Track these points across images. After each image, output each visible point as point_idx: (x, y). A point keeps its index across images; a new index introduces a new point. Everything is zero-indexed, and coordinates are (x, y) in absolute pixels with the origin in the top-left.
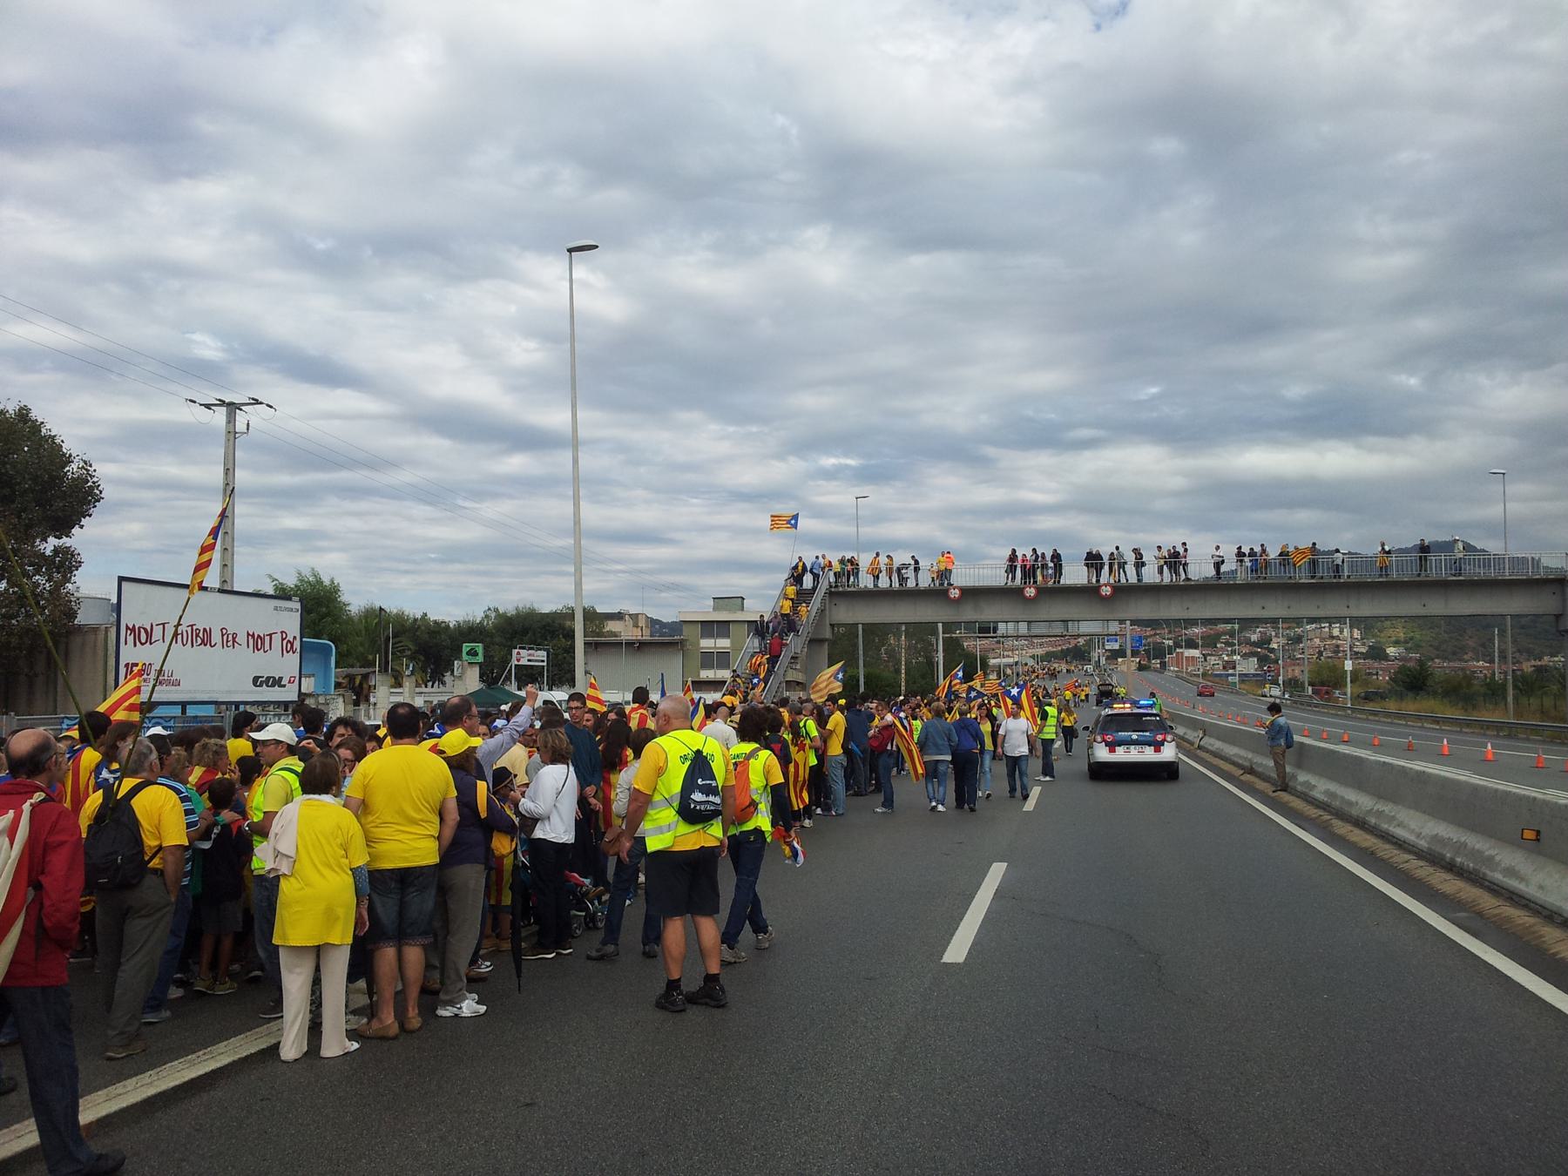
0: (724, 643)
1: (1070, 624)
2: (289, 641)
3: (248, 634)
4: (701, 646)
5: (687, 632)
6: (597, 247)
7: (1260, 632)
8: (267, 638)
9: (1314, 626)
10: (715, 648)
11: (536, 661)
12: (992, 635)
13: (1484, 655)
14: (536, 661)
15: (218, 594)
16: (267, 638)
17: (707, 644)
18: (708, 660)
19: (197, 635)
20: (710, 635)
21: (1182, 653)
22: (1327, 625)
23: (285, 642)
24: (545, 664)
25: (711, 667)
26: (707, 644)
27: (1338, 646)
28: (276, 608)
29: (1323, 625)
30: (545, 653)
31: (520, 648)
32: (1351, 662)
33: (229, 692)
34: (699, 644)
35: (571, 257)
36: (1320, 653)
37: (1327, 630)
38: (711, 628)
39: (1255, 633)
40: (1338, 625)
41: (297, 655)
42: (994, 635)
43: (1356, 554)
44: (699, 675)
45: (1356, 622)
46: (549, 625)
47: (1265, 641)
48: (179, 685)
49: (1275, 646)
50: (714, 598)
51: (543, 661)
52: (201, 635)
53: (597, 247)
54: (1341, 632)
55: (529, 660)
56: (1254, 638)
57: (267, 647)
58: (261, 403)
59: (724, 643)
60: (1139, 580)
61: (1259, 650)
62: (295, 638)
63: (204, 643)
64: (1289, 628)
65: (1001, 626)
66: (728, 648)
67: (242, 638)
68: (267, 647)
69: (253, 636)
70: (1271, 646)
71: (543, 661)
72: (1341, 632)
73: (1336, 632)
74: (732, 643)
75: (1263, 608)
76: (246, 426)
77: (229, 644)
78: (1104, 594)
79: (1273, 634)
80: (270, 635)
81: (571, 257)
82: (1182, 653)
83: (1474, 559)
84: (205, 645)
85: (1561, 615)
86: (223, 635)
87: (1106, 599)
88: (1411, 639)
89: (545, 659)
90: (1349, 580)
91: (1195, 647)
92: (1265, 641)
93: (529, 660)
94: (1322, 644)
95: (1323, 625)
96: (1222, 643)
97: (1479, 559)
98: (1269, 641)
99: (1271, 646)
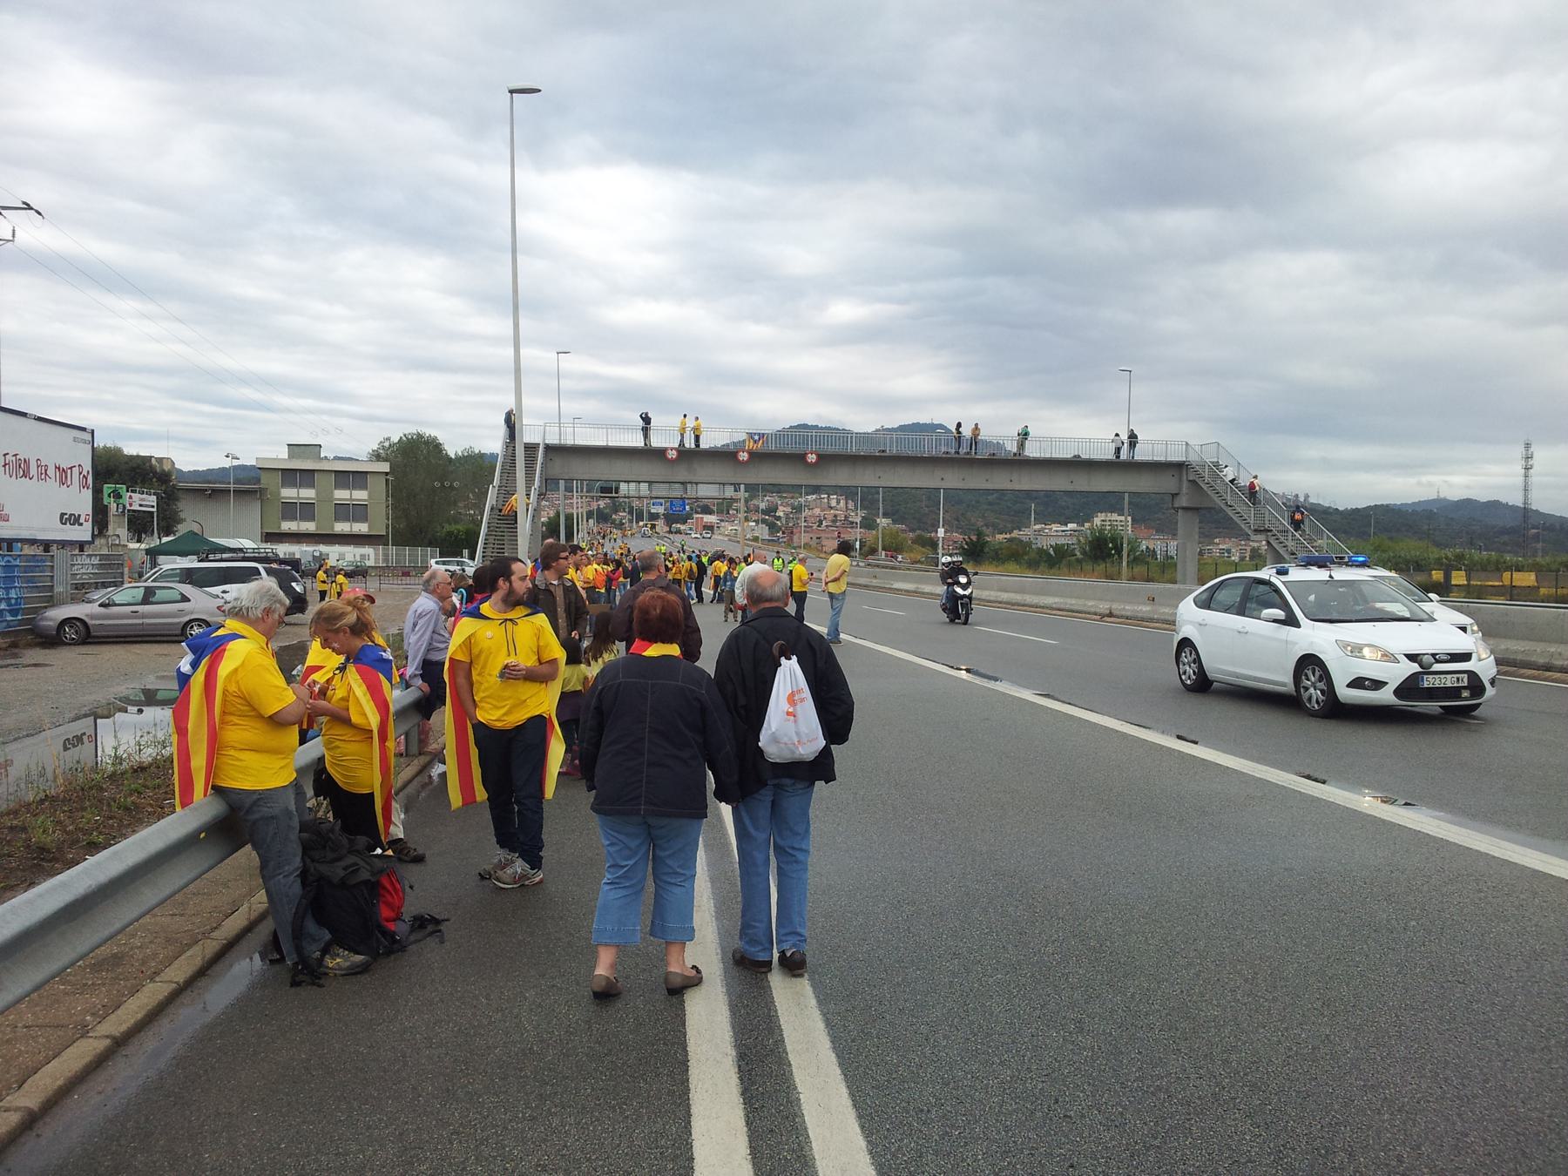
0: (308, 494)
1: (689, 486)
2: (84, 476)
3: (56, 467)
4: (283, 495)
5: (266, 480)
6: (540, 91)
7: (768, 500)
8: (69, 471)
9: (814, 497)
10: (351, 499)
11: (146, 506)
12: (614, 495)
13: (957, 527)
14: (146, 506)
15: (33, 421)
16: (69, 471)
17: (289, 493)
18: (291, 510)
19: (20, 467)
20: (345, 486)
21: (702, 518)
22: (826, 496)
23: (81, 476)
24: (155, 510)
25: (294, 518)
26: (289, 493)
27: (835, 516)
28: (75, 439)
29: (822, 496)
30: (155, 497)
31: (132, 491)
32: (943, 530)
33: (44, 530)
34: (279, 493)
35: (512, 98)
36: (821, 522)
37: (826, 500)
38: (290, 476)
39: (763, 501)
40: (835, 496)
41: (90, 491)
42: (617, 495)
43: (843, 430)
44: (333, 528)
45: (848, 492)
46: (138, 467)
47: (771, 510)
48: (8, 520)
49: (781, 514)
50: (288, 445)
51: (153, 507)
52: (22, 466)
53: (540, 91)
54: (838, 502)
55: (141, 505)
56: (763, 506)
57: (69, 483)
58: (32, 209)
59: (308, 494)
60: (646, 444)
61: (767, 517)
62: (88, 472)
63: (25, 475)
64: (792, 498)
65: (623, 486)
66: (365, 500)
67: (51, 472)
68: (69, 483)
69: (59, 468)
70: (777, 514)
71: (153, 507)
72: (838, 502)
73: (833, 503)
74: (370, 495)
75: (942, 479)
76: (11, 233)
77: (43, 476)
78: (809, 461)
79: (779, 502)
80: (71, 468)
81: (512, 98)
82: (702, 518)
83: (800, 435)
84: (26, 477)
85: (1177, 494)
86: (38, 467)
87: (672, 461)
88: (897, 511)
89: (155, 504)
90: (1015, 458)
91: (710, 512)
92: (771, 510)
93: (141, 505)
94: (822, 514)
95: (822, 496)
96: (734, 509)
97: (796, 435)
98: (776, 510)
99: (777, 514)
